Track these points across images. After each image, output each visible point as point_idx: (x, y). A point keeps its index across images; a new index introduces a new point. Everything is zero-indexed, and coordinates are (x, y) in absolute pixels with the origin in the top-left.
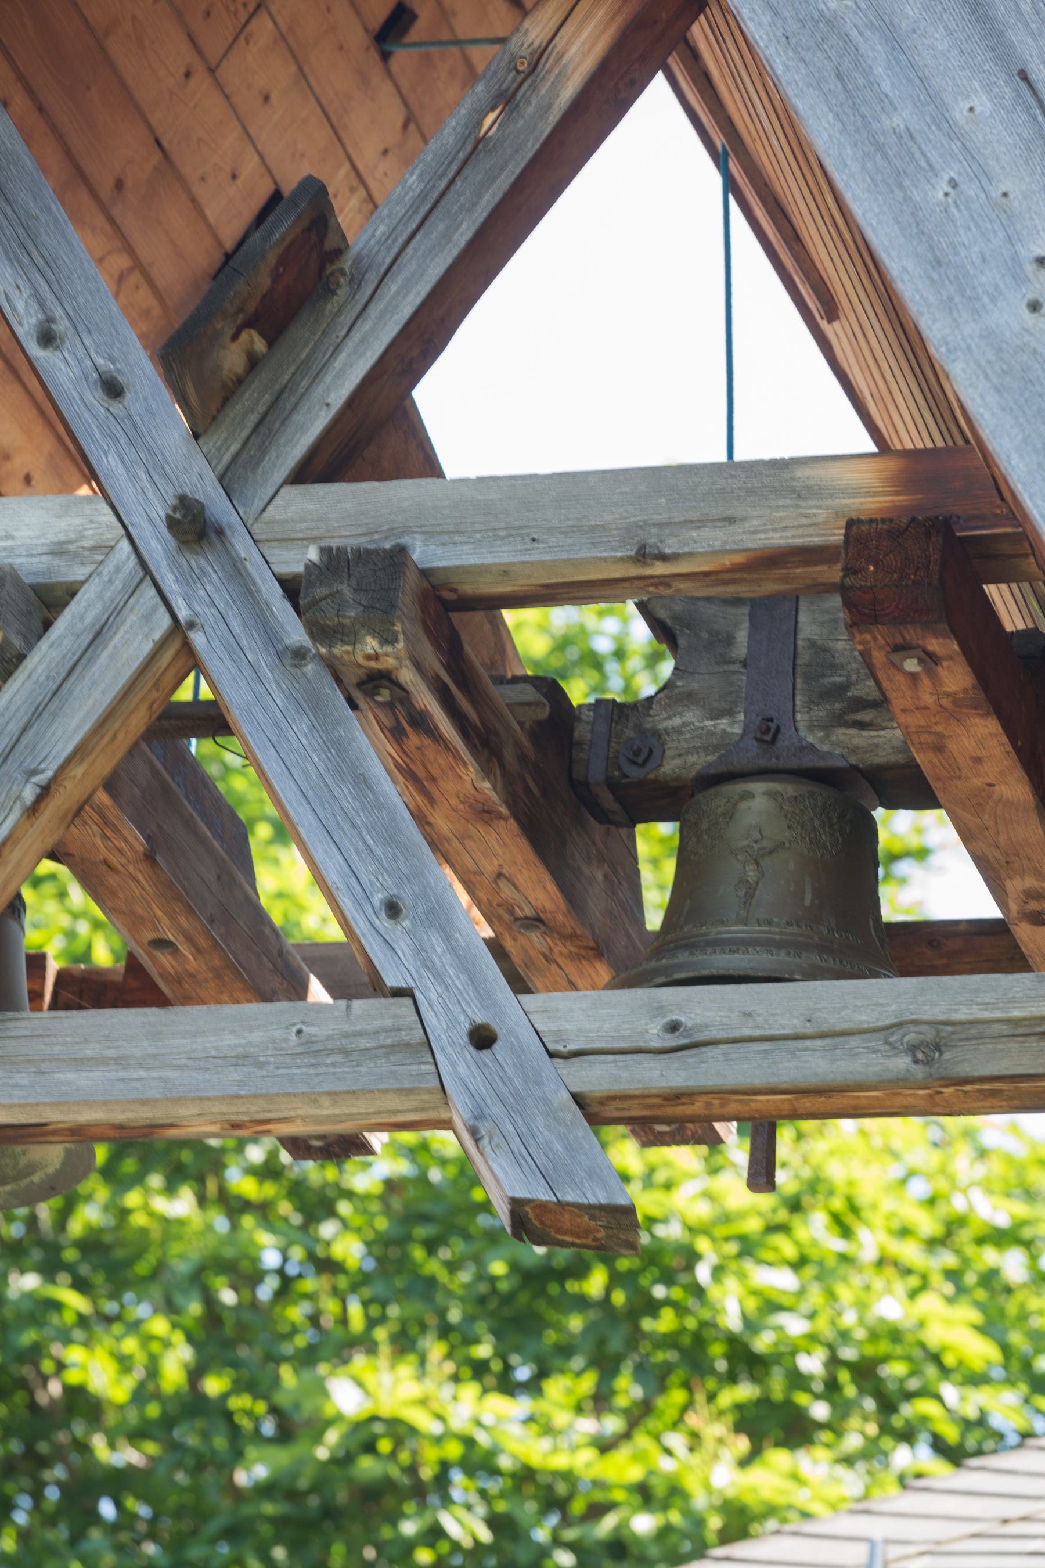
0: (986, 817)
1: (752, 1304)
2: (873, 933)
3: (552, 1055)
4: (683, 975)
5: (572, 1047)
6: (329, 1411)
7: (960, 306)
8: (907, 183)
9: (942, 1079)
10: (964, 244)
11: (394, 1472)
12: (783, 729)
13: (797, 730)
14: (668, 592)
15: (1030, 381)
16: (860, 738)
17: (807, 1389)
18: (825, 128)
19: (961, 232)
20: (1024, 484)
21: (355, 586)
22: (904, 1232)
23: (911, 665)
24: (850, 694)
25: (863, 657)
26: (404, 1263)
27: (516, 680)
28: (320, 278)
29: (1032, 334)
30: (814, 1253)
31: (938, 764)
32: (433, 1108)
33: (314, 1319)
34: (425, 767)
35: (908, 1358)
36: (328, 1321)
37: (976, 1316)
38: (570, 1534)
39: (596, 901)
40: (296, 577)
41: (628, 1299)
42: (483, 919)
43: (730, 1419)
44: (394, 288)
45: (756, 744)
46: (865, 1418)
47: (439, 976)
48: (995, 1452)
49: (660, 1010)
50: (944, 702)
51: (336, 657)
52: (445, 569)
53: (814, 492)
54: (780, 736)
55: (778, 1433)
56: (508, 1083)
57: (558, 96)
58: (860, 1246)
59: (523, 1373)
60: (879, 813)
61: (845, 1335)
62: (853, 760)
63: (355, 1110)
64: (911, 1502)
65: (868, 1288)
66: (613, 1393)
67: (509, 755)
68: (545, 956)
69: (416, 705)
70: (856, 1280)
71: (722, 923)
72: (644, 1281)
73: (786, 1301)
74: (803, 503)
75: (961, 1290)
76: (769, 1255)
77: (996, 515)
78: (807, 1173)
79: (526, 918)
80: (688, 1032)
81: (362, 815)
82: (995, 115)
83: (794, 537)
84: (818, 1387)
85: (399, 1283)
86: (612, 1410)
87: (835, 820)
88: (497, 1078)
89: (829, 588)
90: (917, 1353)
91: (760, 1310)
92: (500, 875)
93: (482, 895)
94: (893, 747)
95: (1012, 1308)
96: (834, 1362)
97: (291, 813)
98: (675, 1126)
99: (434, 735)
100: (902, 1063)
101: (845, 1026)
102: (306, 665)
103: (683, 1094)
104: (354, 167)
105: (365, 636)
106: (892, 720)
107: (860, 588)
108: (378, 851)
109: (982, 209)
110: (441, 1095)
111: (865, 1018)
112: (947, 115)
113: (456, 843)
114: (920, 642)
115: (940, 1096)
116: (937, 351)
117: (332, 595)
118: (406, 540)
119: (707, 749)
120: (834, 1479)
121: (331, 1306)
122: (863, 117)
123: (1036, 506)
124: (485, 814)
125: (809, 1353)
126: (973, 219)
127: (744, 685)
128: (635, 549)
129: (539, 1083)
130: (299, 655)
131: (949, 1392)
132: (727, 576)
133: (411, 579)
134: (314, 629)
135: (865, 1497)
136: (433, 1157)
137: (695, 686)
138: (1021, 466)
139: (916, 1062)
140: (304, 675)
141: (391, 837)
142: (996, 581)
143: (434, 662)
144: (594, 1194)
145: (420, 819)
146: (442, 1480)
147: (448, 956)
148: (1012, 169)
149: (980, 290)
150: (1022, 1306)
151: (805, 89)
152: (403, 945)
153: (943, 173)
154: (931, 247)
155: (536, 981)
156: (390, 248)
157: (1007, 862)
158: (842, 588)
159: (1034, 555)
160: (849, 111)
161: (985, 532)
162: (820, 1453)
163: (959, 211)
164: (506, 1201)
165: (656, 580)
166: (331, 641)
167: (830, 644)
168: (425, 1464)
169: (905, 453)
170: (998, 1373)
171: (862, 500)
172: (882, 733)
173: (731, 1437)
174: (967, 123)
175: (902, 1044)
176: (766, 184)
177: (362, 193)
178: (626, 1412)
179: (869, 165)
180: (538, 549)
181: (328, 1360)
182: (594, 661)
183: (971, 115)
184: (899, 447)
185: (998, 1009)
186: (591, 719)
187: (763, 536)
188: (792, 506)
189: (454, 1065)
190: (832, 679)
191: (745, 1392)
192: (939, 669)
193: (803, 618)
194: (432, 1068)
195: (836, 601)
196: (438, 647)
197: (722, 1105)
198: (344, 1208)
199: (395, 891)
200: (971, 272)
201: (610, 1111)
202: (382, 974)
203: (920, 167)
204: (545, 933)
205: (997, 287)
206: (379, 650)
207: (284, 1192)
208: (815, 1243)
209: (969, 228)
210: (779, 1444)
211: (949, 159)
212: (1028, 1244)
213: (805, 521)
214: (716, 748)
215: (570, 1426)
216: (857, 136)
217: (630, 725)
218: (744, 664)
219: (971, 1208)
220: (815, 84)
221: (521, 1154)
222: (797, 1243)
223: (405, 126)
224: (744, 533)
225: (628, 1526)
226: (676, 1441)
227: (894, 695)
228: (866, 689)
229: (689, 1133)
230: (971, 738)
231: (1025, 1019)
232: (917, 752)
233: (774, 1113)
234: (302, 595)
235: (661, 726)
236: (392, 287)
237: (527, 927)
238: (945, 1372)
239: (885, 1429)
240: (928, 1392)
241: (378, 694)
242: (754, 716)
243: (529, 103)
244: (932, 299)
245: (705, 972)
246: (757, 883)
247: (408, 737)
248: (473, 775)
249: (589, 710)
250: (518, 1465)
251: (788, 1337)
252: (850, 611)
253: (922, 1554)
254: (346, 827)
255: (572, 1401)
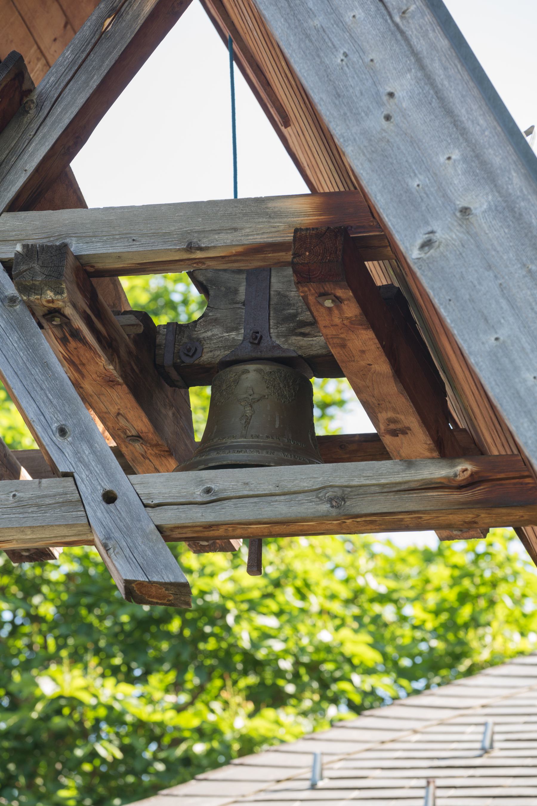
0: (368, 381)
1: (255, 635)
2: (311, 441)
3: (145, 506)
4: (213, 464)
5: (156, 501)
6: (38, 693)
7: (350, 118)
8: (322, 54)
9: (345, 515)
10: (351, 86)
11: (71, 724)
12: (264, 338)
13: (271, 338)
14: (203, 267)
15: (386, 156)
16: (303, 341)
17: (284, 678)
18: (279, 26)
19: (350, 79)
20: (383, 209)
21: (41, 265)
22: (333, 597)
23: (328, 303)
24: (298, 319)
25: (303, 299)
26: (76, 617)
27: (126, 313)
28: (21, 105)
29: (387, 132)
30: (287, 608)
31: (343, 355)
32: (84, 534)
33: (30, 646)
34: (79, 358)
35: (335, 661)
36: (37, 648)
37: (369, 639)
38: (162, 755)
39: (169, 428)
40: (10, 260)
41: (191, 633)
42: (111, 437)
43: (244, 694)
44: (59, 110)
45: (250, 345)
46: (313, 692)
47: (87, 466)
48: (380, 707)
49: (201, 482)
50: (345, 322)
51: (32, 302)
52: (87, 255)
53: (278, 214)
54: (262, 341)
55: (269, 700)
56: (123, 521)
57: (143, 10)
58: (311, 604)
59: (138, 672)
60: (314, 380)
61: (302, 650)
62: (300, 353)
63: (44, 536)
64: (335, 734)
65: (314, 625)
66: (184, 682)
67: (123, 351)
68: (142, 455)
69: (74, 326)
70: (309, 622)
71: (233, 437)
72: (200, 624)
73: (272, 633)
74: (272, 220)
75: (362, 625)
76: (264, 610)
77: (370, 226)
78: (283, 567)
79: (133, 436)
80: (216, 493)
81: (46, 383)
82: (366, 19)
83: (267, 238)
84: (289, 676)
85: (73, 627)
86: (184, 690)
87: (291, 384)
88: (117, 518)
89: (286, 264)
90: (340, 658)
91: (259, 637)
92: (119, 414)
93: (109, 424)
94: (320, 346)
95: (387, 634)
96: (297, 663)
97: (9, 382)
98: (211, 542)
99: (83, 342)
100: (325, 508)
101: (296, 489)
102: (16, 306)
103: (213, 525)
104: (39, 48)
105: (47, 290)
106: (319, 332)
107: (302, 264)
108: (55, 402)
109: (361, 68)
110: (88, 527)
111: (306, 485)
112: (342, 19)
113: (96, 397)
114: (333, 291)
115: (344, 524)
116: (339, 141)
117: (29, 269)
118: (67, 241)
119: (224, 348)
120: (297, 723)
121: (38, 640)
122: (299, 20)
123: (390, 220)
124: (111, 382)
125: (285, 659)
126: (356, 73)
127: (244, 315)
128: (186, 244)
129: (139, 521)
130: (12, 300)
131: (356, 678)
132: (233, 258)
133: (70, 261)
134: (20, 287)
135: (314, 731)
136: (91, 562)
137: (218, 315)
138: (382, 200)
139: (332, 507)
140: (15, 311)
141: (61, 394)
142: (372, 260)
143: (83, 303)
144: (168, 577)
145: (77, 385)
146: (96, 728)
147: (91, 455)
148: (375, 47)
149: (360, 110)
150: (393, 633)
151: (269, 6)
152: (68, 450)
153: (340, 49)
154: (335, 87)
155: (138, 468)
156: (57, 89)
157: (379, 404)
158: (292, 264)
159: (390, 246)
160: (292, 17)
161: (365, 235)
162: (290, 710)
163: (349, 69)
164: (122, 582)
165: (197, 261)
166: (29, 293)
167: (288, 294)
168: (88, 720)
169: (325, 194)
170: (380, 668)
171: (302, 218)
172: (315, 339)
173: (244, 703)
174: (352, 24)
175: (325, 498)
176: (252, 56)
177: (43, 61)
178: (191, 691)
179: (302, 45)
180: (136, 245)
181: (37, 667)
182: (172, 306)
183: (354, 19)
184: (322, 191)
185: (373, 479)
186: (165, 333)
187: (252, 237)
188: (266, 222)
189: (95, 512)
190: (289, 311)
191: (252, 680)
192: (343, 305)
193: (273, 280)
194: (84, 513)
195: (289, 271)
196: (85, 296)
197: (233, 530)
198: (45, 589)
199: (64, 423)
200: (355, 100)
201: (176, 534)
202: (57, 465)
203: (329, 46)
204: (142, 443)
205: (368, 108)
206: (54, 298)
207: (13, 581)
208: (287, 603)
209: (354, 78)
210: (268, 706)
211: (343, 42)
212: (396, 602)
213: (273, 230)
214: (230, 347)
215: (162, 699)
216: (296, 30)
217: (185, 336)
218: (244, 304)
219: (367, 584)
220: (274, 3)
221: (130, 557)
222: (278, 603)
223: (65, 26)
224: (242, 236)
225: (191, 750)
226: (217, 706)
227: (320, 319)
228: (306, 316)
229: (218, 545)
230: (360, 341)
231: (387, 484)
232: (332, 348)
233: (260, 534)
234: (13, 270)
235: (201, 336)
236: (58, 109)
237: (133, 441)
238: (354, 667)
239: (323, 697)
240: (342, 678)
241: (54, 321)
242: (249, 331)
243: (128, 14)
244: (335, 114)
245: (225, 463)
246: (251, 416)
247: (70, 343)
248: (104, 362)
249: (164, 328)
250: (136, 719)
251: (273, 651)
252: (297, 276)
253: (341, 760)
254: (38, 389)
255: (163, 686)
